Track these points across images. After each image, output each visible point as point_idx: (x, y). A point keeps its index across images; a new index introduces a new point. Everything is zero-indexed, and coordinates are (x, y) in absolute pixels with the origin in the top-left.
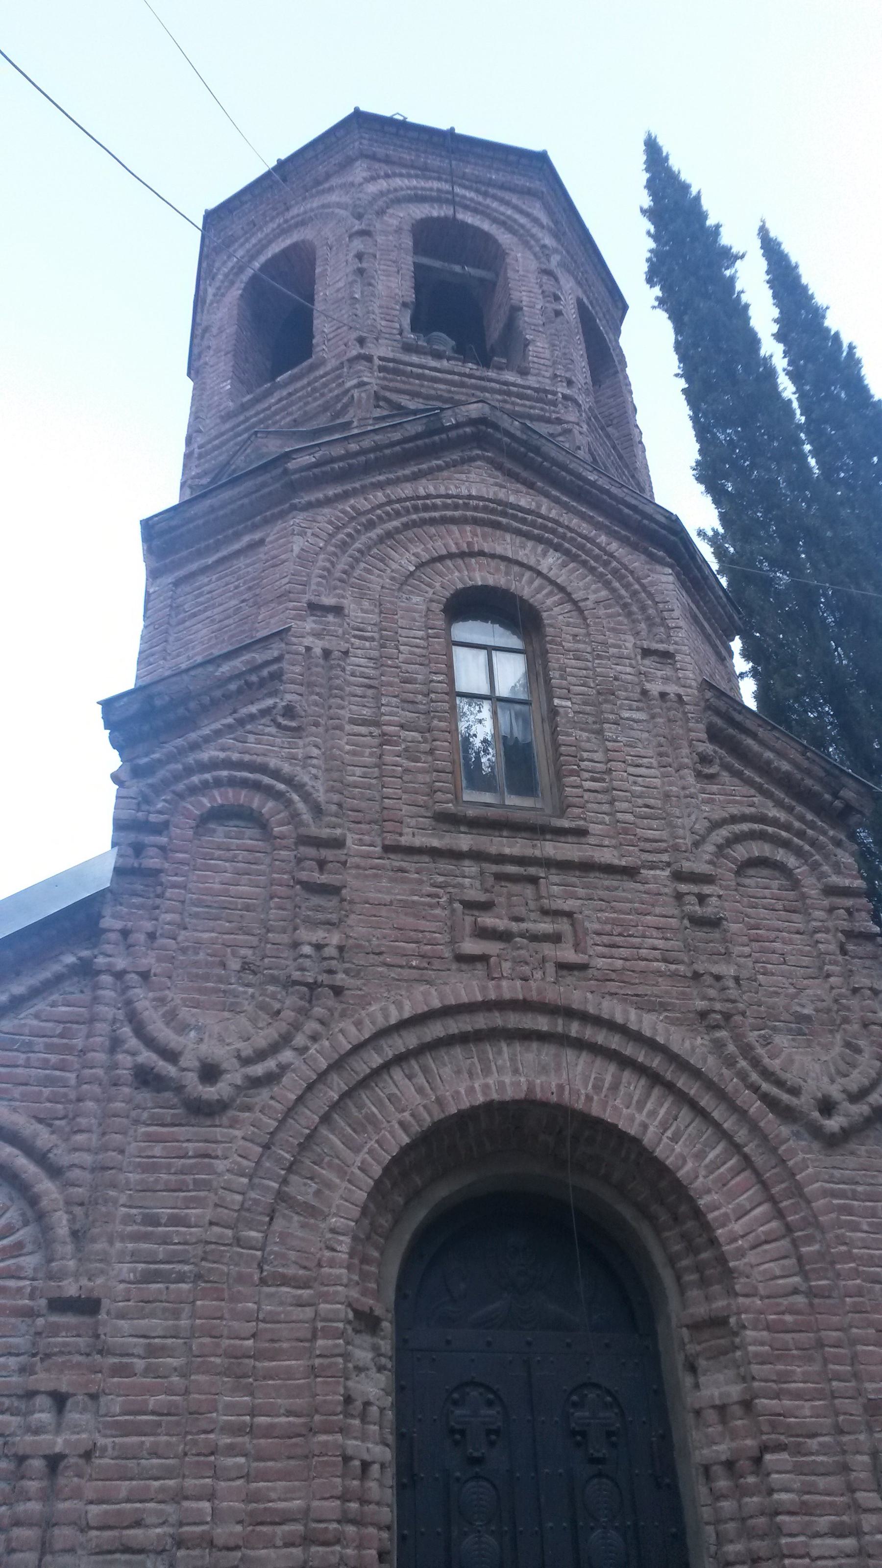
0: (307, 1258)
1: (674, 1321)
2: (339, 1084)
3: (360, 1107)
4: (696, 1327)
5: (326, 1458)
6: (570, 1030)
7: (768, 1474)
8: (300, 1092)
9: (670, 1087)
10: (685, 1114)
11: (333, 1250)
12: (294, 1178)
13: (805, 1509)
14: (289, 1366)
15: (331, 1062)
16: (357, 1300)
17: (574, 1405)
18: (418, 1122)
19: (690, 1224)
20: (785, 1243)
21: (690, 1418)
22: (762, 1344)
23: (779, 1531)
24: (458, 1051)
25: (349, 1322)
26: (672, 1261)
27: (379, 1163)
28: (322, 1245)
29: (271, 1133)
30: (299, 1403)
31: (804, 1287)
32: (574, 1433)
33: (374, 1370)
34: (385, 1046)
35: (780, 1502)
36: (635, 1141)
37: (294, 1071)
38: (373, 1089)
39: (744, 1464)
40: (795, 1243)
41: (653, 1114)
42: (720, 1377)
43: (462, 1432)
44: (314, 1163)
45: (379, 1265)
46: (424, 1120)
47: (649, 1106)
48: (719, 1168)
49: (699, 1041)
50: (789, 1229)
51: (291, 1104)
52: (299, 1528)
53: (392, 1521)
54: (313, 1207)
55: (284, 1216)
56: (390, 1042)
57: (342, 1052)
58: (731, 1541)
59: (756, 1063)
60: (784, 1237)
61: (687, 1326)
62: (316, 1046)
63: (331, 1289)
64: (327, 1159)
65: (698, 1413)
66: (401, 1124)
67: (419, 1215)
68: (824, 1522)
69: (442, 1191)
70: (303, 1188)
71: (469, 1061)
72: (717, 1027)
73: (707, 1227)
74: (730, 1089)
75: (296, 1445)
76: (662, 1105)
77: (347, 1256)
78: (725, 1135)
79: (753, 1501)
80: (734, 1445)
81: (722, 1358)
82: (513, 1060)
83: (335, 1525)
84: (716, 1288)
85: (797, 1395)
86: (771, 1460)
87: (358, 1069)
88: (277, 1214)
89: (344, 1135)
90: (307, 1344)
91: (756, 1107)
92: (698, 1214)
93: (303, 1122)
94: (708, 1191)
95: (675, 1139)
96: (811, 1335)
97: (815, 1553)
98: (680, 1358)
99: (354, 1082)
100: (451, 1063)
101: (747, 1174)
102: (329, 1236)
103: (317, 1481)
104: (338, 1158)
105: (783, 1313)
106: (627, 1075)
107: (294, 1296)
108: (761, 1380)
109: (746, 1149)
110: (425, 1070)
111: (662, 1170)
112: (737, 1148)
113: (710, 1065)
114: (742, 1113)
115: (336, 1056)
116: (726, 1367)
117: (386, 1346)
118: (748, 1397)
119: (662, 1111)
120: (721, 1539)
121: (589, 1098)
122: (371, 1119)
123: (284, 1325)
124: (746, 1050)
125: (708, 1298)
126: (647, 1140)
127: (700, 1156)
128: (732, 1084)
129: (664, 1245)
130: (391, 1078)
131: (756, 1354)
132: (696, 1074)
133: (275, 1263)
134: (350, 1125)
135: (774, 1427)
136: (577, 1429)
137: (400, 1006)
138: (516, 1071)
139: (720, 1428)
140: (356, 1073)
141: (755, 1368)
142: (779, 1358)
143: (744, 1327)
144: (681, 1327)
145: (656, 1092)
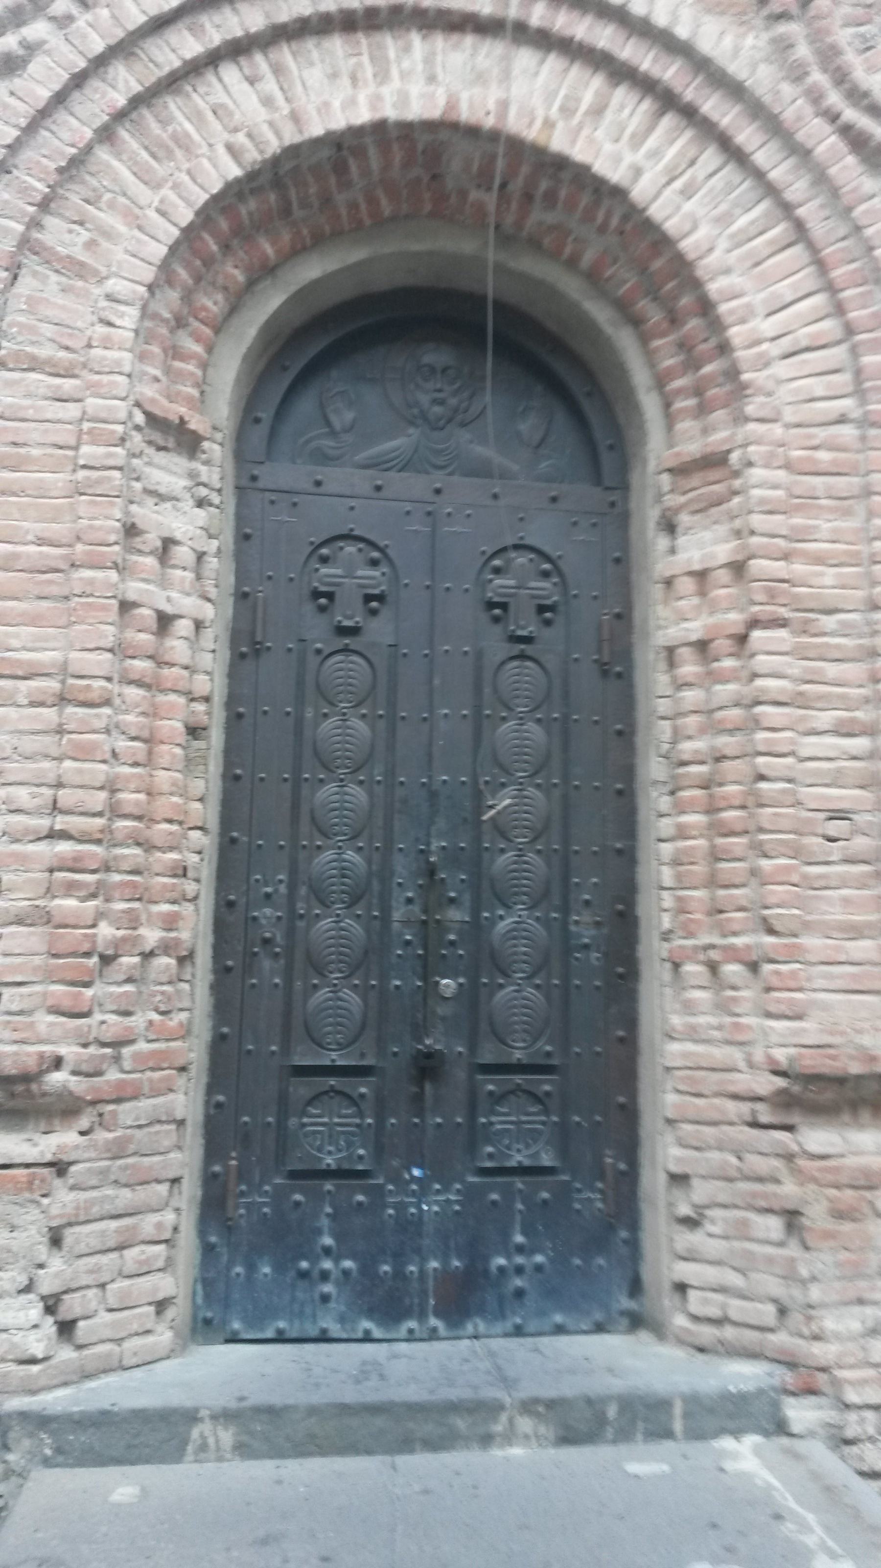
0: (70, 335)
1: (652, 465)
2: (126, 82)
3: (163, 123)
4: (681, 471)
5: (90, 600)
6: (529, 15)
7: (753, 655)
8: (57, 87)
9: (689, 113)
10: (711, 157)
11: (110, 324)
12: (50, 221)
13: (800, 701)
14: (41, 480)
15: (112, 41)
16: (153, 401)
17: (497, 571)
18: (257, 145)
19: (693, 324)
20: (838, 354)
21: (658, 591)
22: (775, 487)
23: (756, 724)
24: (336, 44)
25: (138, 428)
26: (660, 381)
27: (188, 203)
28: (95, 318)
29: (9, 147)
30: (59, 529)
31: (856, 414)
32: (491, 605)
33: (191, 502)
34: (208, 26)
35: (763, 690)
36: (618, 193)
37: (48, 53)
38: (188, 96)
39: (722, 645)
40: (854, 352)
41: (655, 154)
42: (707, 535)
43: (330, 596)
44: (87, 201)
45: (204, 366)
46: (267, 142)
47: (652, 142)
48: (750, 239)
49: (750, 41)
50: (850, 330)
51: (41, 105)
52: (53, 685)
53: (212, 691)
54: (82, 264)
55: (35, 274)
56: (217, 18)
57: (131, 27)
58: (690, 738)
59: (841, 77)
60: (839, 342)
61: (670, 470)
62: (88, 16)
63: (105, 378)
64: (107, 196)
65: (669, 582)
66: (230, 149)
67: (271, 302)
68: (825, 718)
69: (311, 269)
70: (67, 237)
71: (353, 60)
72: (783, 16)
73: (716, 325)
74: (788, 115)
75: (50, 582)
76: (672, 142)
77: (132, 335)
78: (771, 190)
79: (726, 691)
80: (711, 620)
81: (714, 510)
82: (429, 60)
83: (103, 683)
84: (720, 415)
85: (819, 559)
86: (760, 638)
87: (160, 59)
88: (24, 271)
89: (136, 163)
90: (70, 453)
91: (826, 143)
92: (706, 307)
93: (66, 136)
94: (727, 271)
95: (687, 193)
96: (855, 480)
97: (805, 752)
98: (653, 514)
99: (153, 79)
100: (323, 61)
101: (798, 250)
102: (103, 303)
103: (77, 627)
104: (125, 194)
105: (815, 448)
106: (622, 94)
107: (49, 387)
108: (763, 535)
109: (801, 212)
110: (278, 70)
111: (659, 241)
112: (787, 209)
113: (762, 79)
114: (801, 153)
115: (120, 34)
116: (715, 523)
117: (211, 475)
118: (739, 557)
119: (672, 152)
120: (678, 736)
121: (549, 124)
122: (184, 143)
123: (33, 425)
124: (829, 56)
125: (705, 431)
126: (639, 192)
127: (725, 220)
128: (791, 104)
129: (650, 357)
130: (220, 80)
131: (762, 501)
132: (735, 90)
133: (20, 339)
134: (146, 148)
135: (772, 597)
136: (496, 599)
137: (351, 103)
138: (431, 79)
139: (696, 601)
140: (157, 65)
141: (757, 520)
142: (798, 508)
143: (750, 464)
144: (660, 473)
145: (668, 121)
